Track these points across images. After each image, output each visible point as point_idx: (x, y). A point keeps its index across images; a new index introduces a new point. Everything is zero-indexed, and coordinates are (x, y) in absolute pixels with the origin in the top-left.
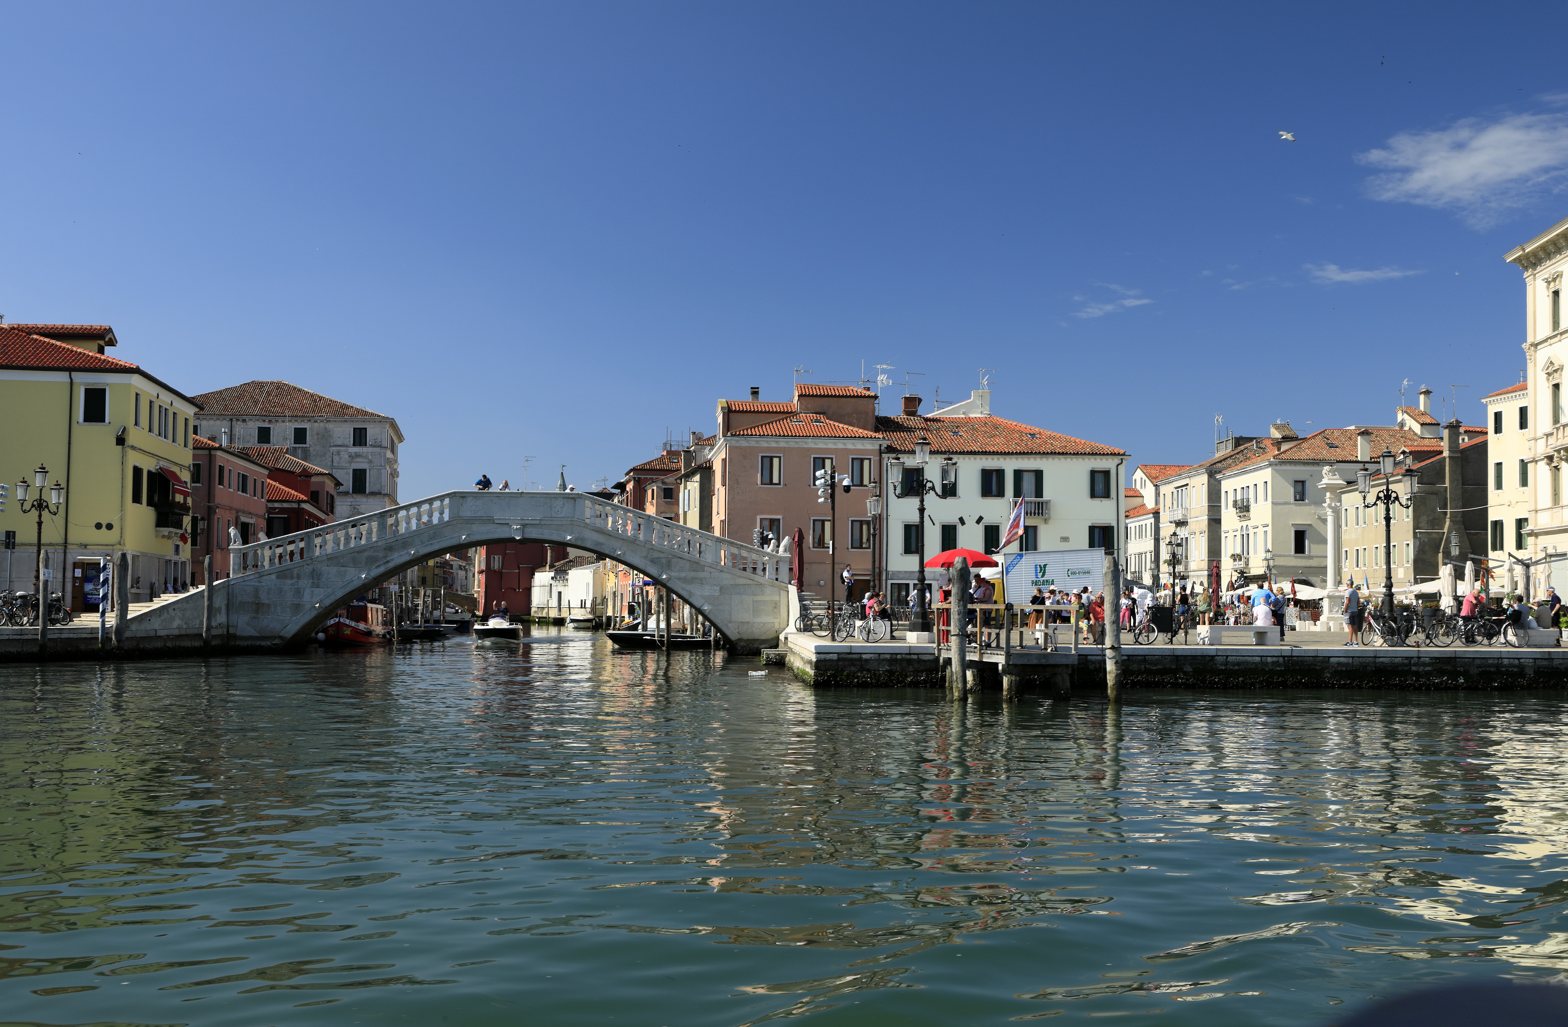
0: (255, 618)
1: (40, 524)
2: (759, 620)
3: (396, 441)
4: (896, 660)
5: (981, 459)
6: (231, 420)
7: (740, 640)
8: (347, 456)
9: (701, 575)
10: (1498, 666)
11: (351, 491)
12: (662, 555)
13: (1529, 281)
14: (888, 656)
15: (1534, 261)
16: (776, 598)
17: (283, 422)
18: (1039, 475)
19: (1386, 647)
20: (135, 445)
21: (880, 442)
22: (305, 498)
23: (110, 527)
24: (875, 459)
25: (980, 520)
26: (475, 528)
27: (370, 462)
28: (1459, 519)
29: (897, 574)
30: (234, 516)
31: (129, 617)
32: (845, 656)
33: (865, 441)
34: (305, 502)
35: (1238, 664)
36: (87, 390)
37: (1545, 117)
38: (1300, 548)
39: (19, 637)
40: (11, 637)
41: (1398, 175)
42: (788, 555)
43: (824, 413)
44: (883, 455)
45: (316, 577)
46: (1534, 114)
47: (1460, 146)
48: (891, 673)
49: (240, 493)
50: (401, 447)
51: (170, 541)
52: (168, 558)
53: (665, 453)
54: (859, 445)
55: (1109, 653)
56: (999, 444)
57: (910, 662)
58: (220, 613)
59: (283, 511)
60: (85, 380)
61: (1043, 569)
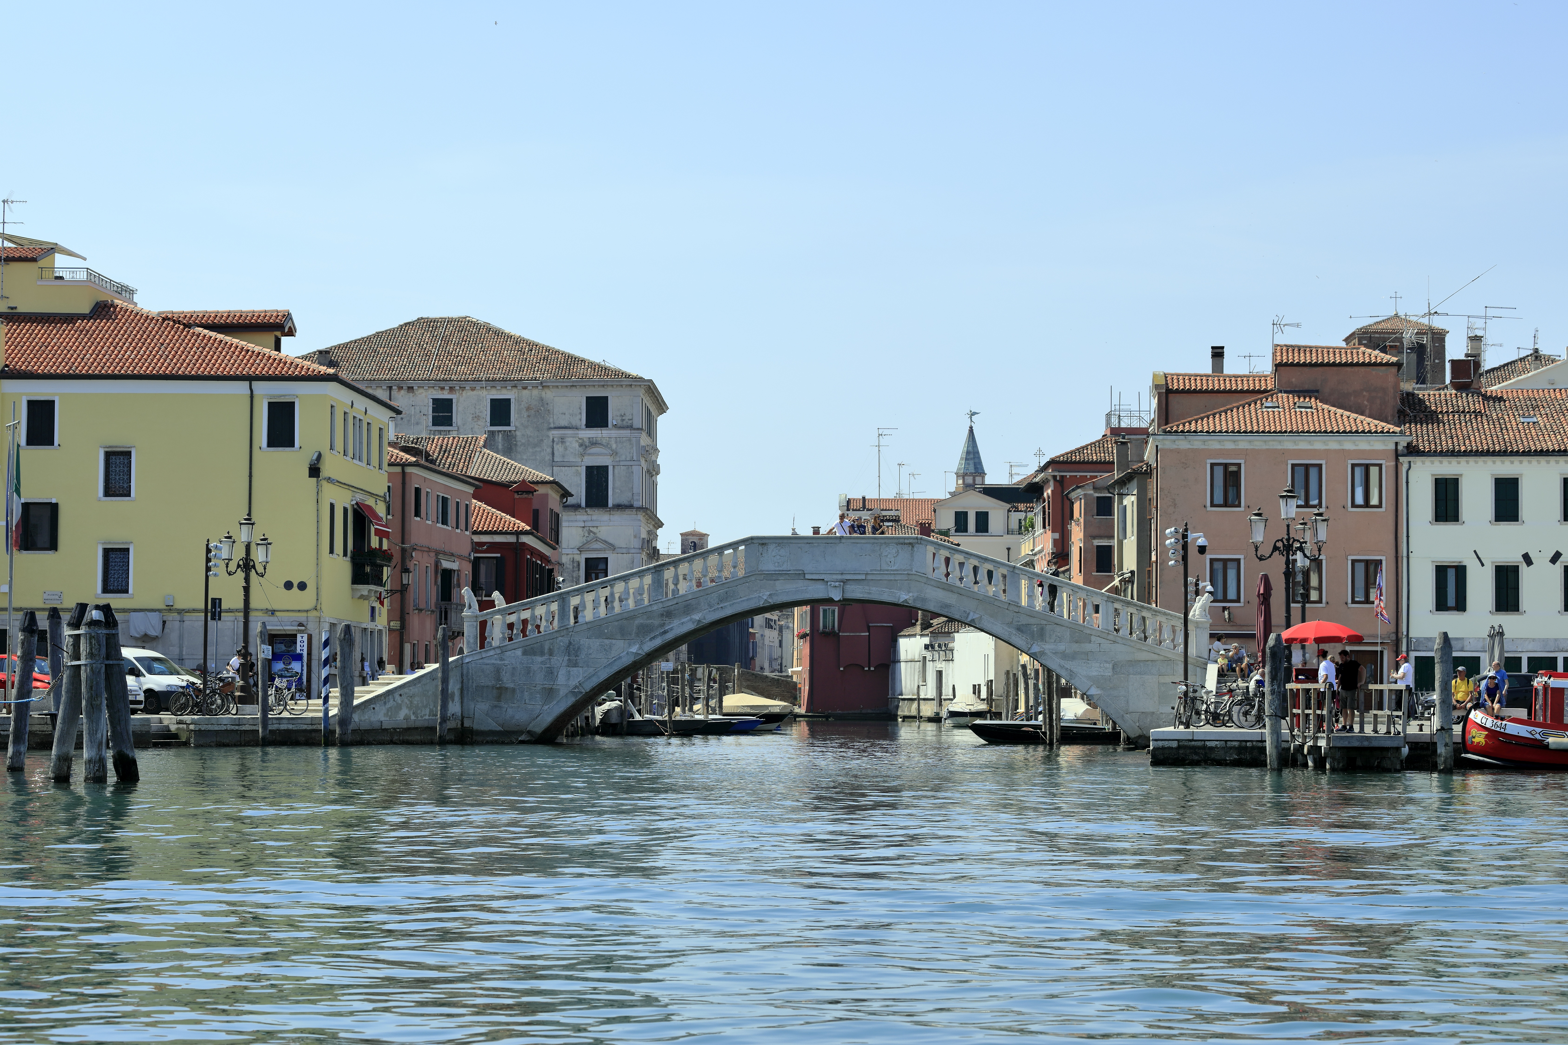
0: (496, 706)
1: (247, 589)
3: (654, 411)
4: (1246, 747)
5: (1557, 462)
6: (390, 388)
8: (576, 445)
9: (1087, 647)
11: (583, 504)
14: (1236, 744)
17: (473, 389)
20: (333, 477)
21: (1396, 439)
22: (528, 528)
23: (302, 586)
24: (1388, 464)
26: (780, 585)
27: (615, 453)
30: (433, 561)
31: (356, 702)
32: (1186, 743)
33: (1373, 438)
34: (526, 533)
36: (271, 405)
39: (237, 728)
40: (229, 728)
44: (1401, 459)
45: (572, 652)
49: (440, 525)
50: (662, 422)
51: (366, 602)
52: (364, 626)
54: (1363, 444)
57: (1194, 748)
58: (453, 701)
59: (493, 547)
60: (267, 391)
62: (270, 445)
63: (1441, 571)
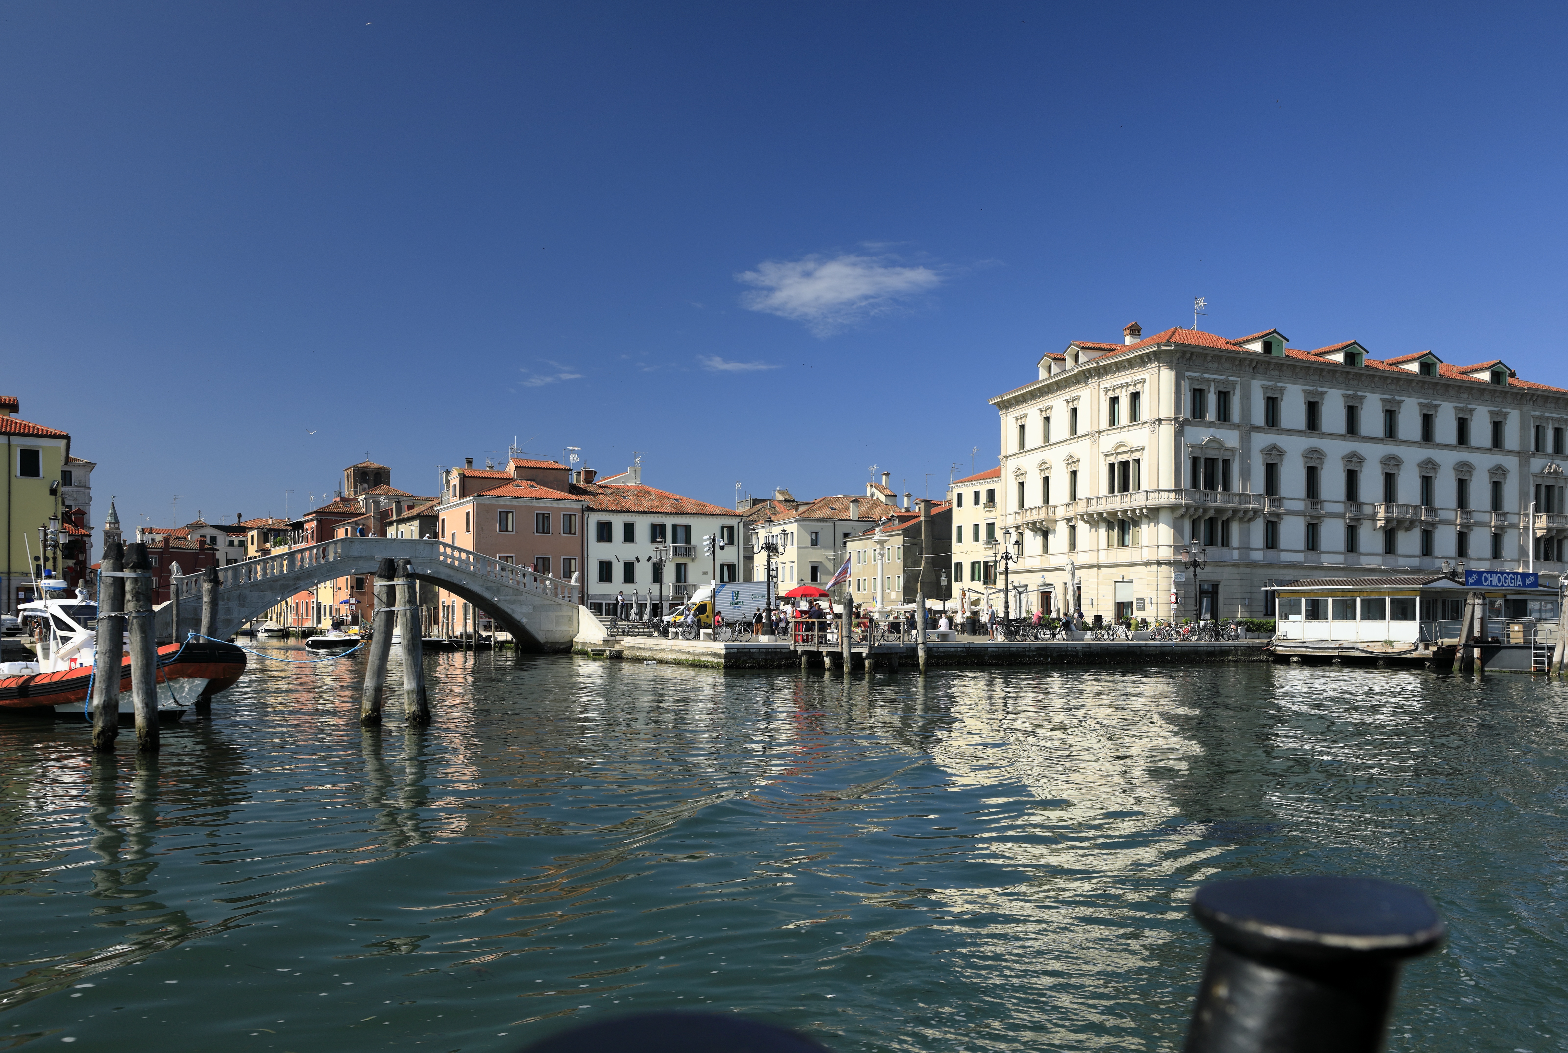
2: (558, 629)
7: (547, 642)
9: (520, 598)
10: (1066, 651)
12: (493, 584)
13: (1003, 417)
15: (1006, 405)
16: (571, 614)
18: (688, 528)
19: (1007, 642)
24: (579, 515)
25: (649, 559)
28: (930, 561)
29: (594, 596)
33: (573, 503)
35: (944, 652)
37: (865, 258)
38: (814, 578)
41: (765, 292)
42: (578, 584)
43: (534, 480)
46: (858, 256)
47: (808, 275)
48: (766, 660)
53: (338, 499)
54: (568, 505)
55: (920, 646)
56: (658, 506)
57: (776, 653)
60: (19, 443)
61: (737, 594)
62: (21, 475)
63: (601, 564)
